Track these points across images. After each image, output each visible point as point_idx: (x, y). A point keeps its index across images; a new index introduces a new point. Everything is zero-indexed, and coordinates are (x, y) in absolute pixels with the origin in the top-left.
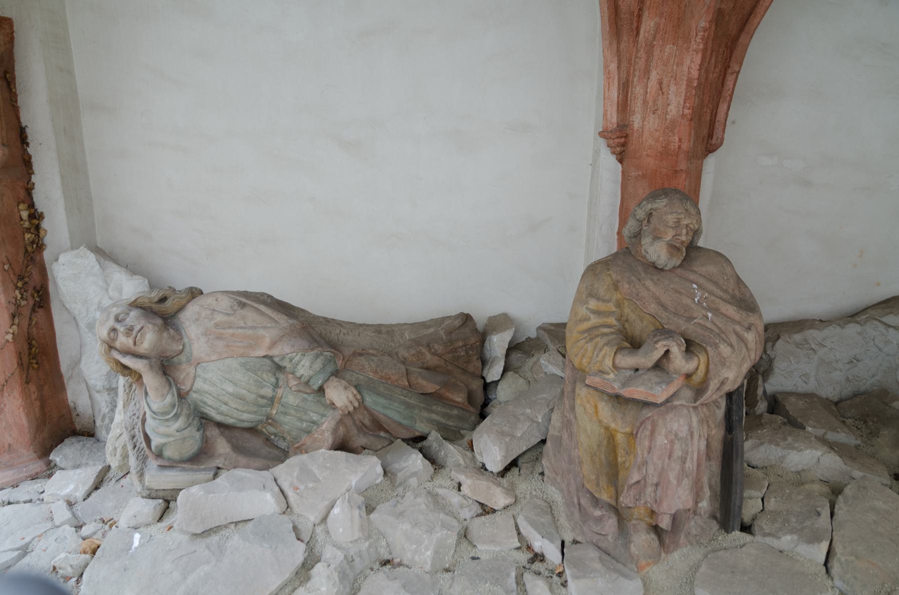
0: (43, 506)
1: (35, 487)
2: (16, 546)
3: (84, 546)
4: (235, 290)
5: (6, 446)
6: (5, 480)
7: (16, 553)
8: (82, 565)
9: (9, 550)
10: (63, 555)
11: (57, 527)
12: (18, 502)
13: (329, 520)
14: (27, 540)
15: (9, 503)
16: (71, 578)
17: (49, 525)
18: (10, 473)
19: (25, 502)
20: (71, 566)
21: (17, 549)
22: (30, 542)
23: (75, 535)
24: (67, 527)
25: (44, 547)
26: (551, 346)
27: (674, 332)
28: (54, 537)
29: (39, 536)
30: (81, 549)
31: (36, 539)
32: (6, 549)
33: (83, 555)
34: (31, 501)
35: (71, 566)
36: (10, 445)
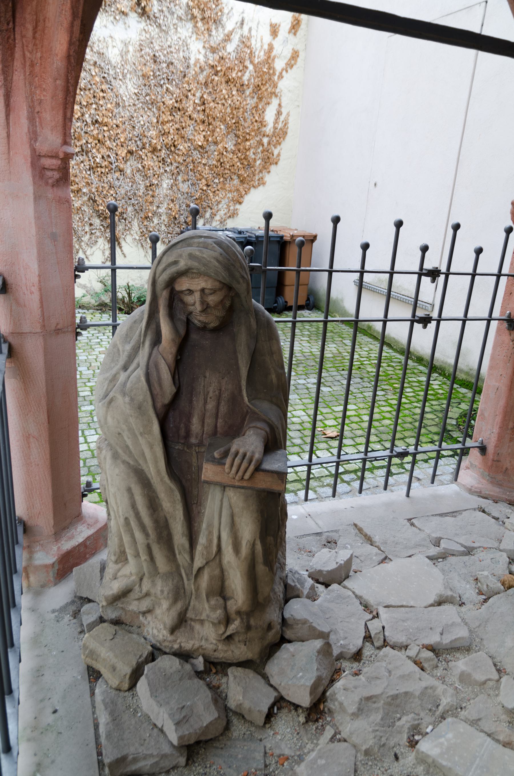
0: (502, 528)
1: (507, 511)
2: (466, 544)
3: (506, 578)
4: (4, 110)
5: (504, 469)
6: (491, 493)
7: (463, 549)
8: (495, 592)
9: (460, 544)
10: (486, 573)
11: (501, 551)
12: (489, 515)
13: (387, 639)
14: (475, 545)
15: (484, 511)
16: (483, 594)
17: (496, 545)
18: (497, 490)
19: (494, 518)
20: (487, 585)
21: (465, 547)
22: (476, 548)
23: (506, 565)
24: (505, 555)
25: (481, 558)
26: (77, 257)
27: (218, 737)
28: (492, 556)
29: (484, 548)
30: (502, 578)
31: (481, 549)
32: (459, 542)
33: (500, 585)
34: (497, 519)
35: (487, 585)
36: (507, 469)
